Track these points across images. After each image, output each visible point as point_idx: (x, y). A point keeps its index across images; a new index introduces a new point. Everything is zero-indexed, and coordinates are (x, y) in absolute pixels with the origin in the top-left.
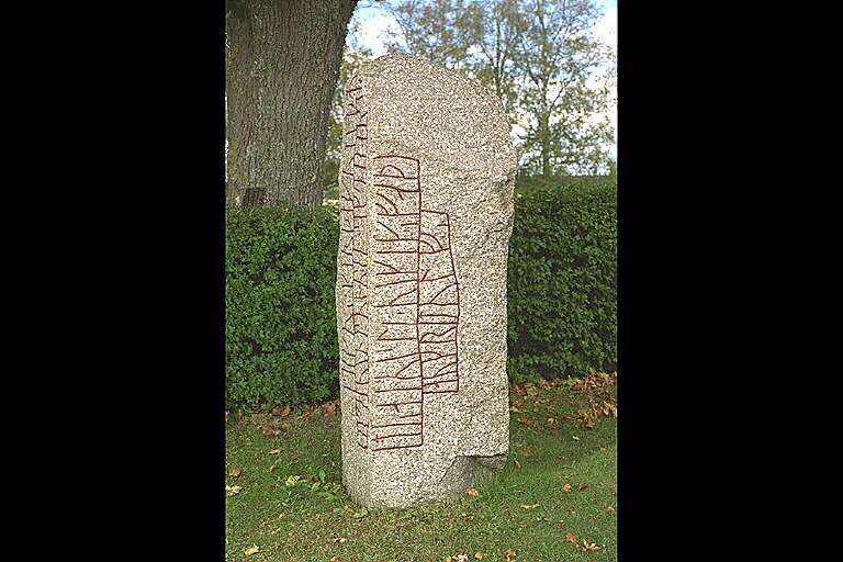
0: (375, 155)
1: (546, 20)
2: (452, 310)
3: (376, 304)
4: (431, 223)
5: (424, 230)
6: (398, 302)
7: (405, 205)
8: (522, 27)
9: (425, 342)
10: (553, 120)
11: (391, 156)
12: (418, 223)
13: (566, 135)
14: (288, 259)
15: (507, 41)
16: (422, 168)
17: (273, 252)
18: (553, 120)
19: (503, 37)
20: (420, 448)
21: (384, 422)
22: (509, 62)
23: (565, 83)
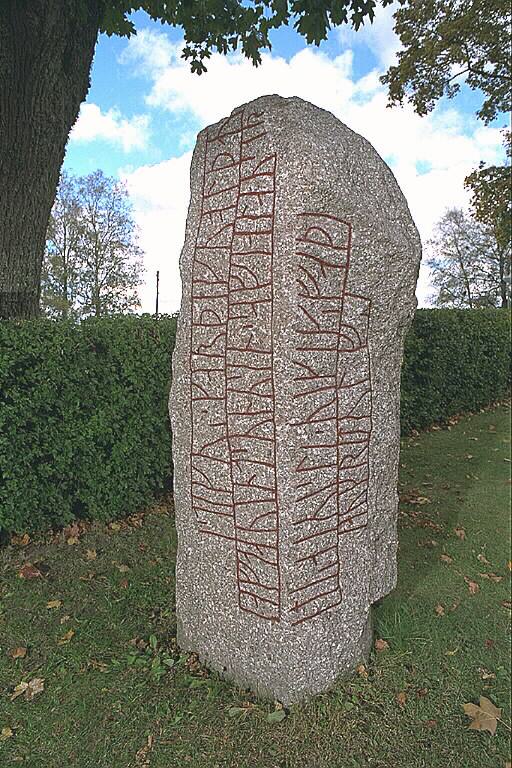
0: (301, 210)
1: (97, 227)
2: (364, 424)
3: (293, 421)
4: (354, 309)
5: (346, 319)
6: (318, 416)
7: (327, 286)
8: (81, 230)
9: (344, 468)
10: (103, 292)
11: (319, 215)
12: (341, 311)
13: (111, 303)
14: (32, 375)
15: (72, 240)
16: (353, 235)
17: (17, 365)
18: (103, 292)
19: (67, 236)
20: (339, 606)
21: (302, 583)
22: (73, 253)
23: (109, 269)
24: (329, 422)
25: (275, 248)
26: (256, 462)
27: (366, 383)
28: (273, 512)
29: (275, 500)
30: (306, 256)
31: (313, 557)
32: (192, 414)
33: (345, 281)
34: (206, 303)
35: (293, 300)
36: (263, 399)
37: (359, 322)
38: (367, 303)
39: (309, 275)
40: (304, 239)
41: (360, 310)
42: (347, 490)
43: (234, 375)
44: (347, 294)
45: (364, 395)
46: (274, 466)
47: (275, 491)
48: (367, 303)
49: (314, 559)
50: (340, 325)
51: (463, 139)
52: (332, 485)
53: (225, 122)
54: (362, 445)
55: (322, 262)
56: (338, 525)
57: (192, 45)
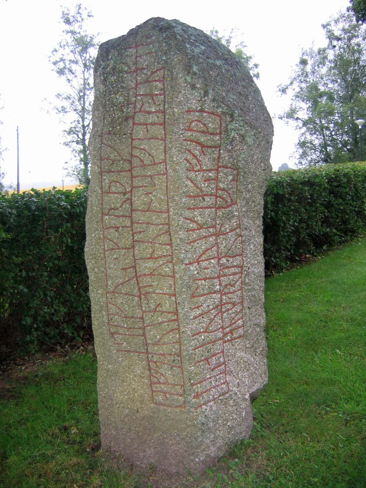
3: (187, 262)
20: (227, 395)
24: (212, 261)
25: (167, 136)
26: (161, 294)
27: (238, 230)
28: (176, 329)
29: (177, 320)
30: (191, 141)
31: (207, 359)
32: (106, 262)
33: (219, 158)
34: (114, 177)
35: (182, 173)
36: (163, 247)
37: (230, 186)
38: (235, 172)
39: (193, 155)
40: (189, 129)
41: (231, 178)
42: (229, 310)
43: (139, 230)
44: (220, 167)
45: (236, 239)
46: (175, 295)
47: (176, 313)
48: (235, 172)
49: (208, 361)
50: (217, 190)
51: (284, 95)
52: (217, 307)
53: (123, 38)
54: (237, 277)
55: (203, 146)
56: (223, 336)
57: (93, 52)
